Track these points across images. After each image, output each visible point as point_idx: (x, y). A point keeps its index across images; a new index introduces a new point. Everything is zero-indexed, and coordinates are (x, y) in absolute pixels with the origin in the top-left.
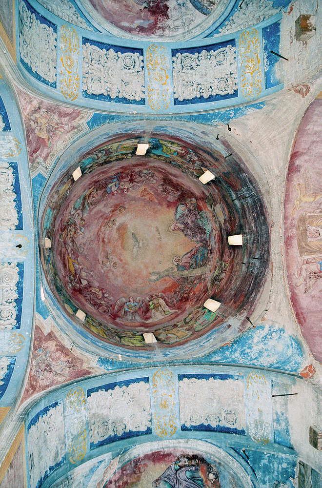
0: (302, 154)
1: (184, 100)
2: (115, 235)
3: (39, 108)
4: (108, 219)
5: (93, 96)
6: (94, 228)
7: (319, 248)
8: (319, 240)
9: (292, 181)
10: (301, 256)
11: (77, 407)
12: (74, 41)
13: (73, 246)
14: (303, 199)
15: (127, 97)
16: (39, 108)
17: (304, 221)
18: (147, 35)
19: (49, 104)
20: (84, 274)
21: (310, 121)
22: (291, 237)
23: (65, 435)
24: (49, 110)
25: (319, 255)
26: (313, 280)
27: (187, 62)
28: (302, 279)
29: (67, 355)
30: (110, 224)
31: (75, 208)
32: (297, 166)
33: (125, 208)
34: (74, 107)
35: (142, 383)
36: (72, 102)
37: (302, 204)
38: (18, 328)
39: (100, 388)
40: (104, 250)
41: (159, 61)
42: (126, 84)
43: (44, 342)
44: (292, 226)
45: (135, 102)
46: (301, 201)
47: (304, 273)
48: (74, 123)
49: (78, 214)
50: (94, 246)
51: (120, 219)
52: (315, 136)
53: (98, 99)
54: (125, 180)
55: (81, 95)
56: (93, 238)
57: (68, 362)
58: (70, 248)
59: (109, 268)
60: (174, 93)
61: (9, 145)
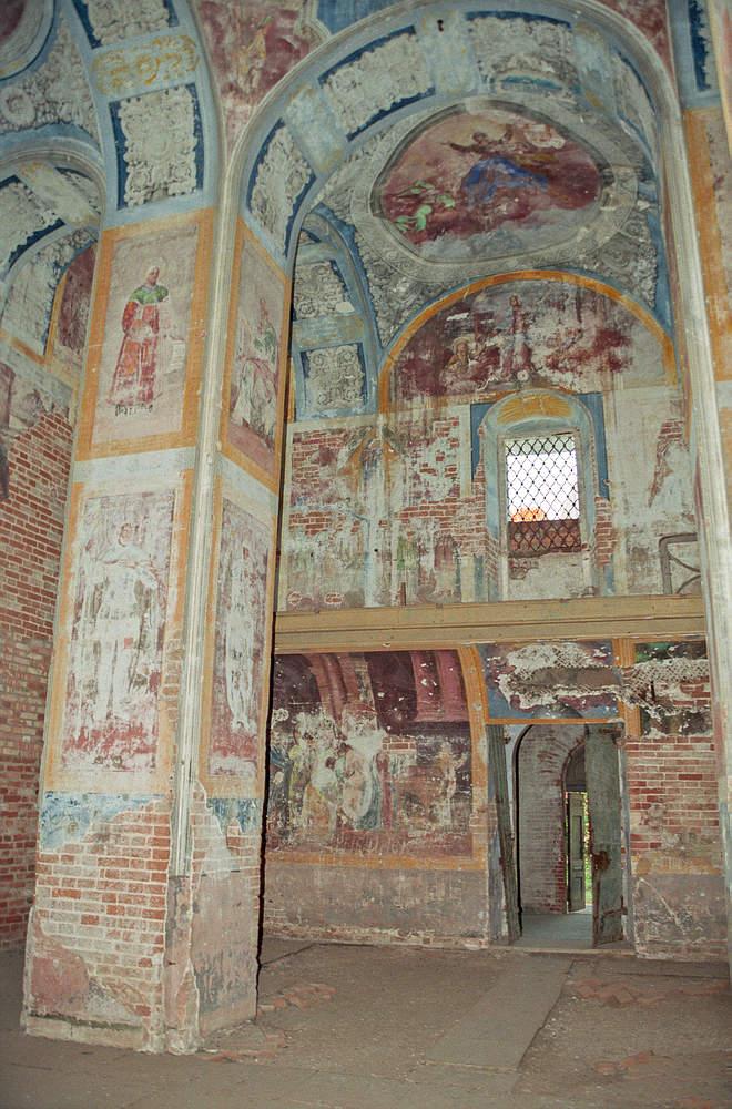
3: (231, 87)
12: (110, 64)
16: (231, 87)
34: (200, 23)
38: (568, 25)
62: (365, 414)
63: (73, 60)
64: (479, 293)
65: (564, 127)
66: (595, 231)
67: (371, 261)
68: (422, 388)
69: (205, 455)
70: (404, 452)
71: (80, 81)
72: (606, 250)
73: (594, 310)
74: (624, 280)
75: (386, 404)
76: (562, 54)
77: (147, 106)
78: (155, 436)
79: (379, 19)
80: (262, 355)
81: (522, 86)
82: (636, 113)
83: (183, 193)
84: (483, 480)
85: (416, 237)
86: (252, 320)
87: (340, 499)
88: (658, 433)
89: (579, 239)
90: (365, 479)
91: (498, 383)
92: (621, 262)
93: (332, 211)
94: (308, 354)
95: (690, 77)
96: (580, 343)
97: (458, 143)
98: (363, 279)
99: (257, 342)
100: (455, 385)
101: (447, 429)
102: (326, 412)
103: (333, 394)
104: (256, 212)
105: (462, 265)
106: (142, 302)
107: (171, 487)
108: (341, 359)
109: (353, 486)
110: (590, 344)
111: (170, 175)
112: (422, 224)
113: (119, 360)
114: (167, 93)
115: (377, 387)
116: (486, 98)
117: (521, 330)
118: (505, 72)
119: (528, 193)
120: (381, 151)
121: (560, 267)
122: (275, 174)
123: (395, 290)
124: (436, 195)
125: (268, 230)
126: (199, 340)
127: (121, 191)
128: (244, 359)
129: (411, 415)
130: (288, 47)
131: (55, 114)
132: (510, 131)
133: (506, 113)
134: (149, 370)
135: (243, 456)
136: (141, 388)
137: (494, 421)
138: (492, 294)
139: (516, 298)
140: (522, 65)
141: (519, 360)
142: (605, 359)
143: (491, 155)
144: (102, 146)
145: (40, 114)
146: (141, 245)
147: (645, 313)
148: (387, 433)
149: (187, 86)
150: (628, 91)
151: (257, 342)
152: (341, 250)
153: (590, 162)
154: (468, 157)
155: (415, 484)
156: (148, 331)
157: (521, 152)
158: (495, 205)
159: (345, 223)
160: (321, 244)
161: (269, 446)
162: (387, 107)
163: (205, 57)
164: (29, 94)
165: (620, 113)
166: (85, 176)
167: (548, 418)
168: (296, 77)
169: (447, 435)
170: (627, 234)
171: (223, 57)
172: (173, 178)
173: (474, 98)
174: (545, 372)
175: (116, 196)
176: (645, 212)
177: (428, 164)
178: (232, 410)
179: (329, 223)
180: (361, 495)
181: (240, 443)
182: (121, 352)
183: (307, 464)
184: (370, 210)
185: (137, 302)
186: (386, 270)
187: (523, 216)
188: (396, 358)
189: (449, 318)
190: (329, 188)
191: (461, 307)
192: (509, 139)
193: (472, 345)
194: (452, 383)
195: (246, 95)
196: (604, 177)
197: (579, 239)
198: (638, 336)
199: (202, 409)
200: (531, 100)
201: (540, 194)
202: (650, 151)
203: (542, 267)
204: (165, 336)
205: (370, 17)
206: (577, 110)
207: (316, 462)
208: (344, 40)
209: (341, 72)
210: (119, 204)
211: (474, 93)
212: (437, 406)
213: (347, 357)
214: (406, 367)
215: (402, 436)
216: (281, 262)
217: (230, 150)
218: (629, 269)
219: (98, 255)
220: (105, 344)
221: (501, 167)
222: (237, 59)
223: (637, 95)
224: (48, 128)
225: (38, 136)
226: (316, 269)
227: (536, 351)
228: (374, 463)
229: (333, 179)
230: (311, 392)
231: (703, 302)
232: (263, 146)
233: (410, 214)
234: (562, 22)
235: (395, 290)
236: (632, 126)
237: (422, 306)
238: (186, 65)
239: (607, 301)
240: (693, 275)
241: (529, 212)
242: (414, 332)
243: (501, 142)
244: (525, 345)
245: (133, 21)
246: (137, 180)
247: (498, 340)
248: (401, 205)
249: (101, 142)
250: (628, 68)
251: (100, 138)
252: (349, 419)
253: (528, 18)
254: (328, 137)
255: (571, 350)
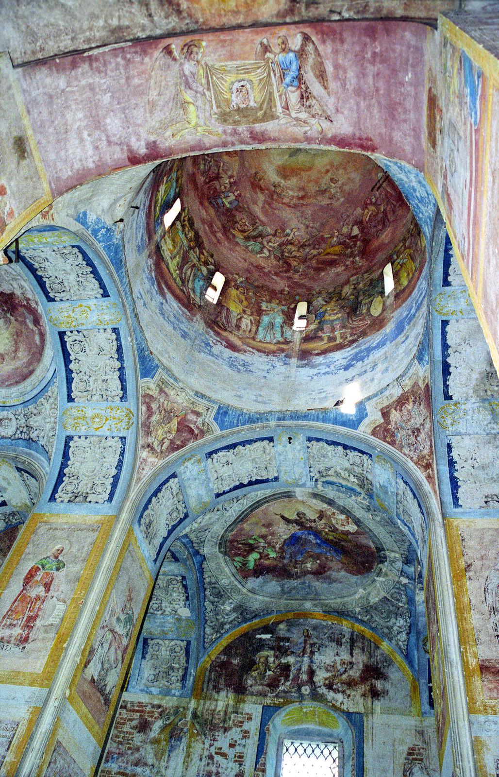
0: (130, 151)
1: (101, 288)
2: (293, 181)
3: (148, 446)
4: (273, 194)
5: (124, 388)
6: (287, 214)
7: (264, 86)
8: (252, 88)
9: (170, 148)
10: (278, 118)
11: (461, 415)
12: (75, 412)
13: (309, 245)
14: (193, 123)
15: (115, 348)
16: (148, 446)
17: (225, 114)
18: (41, 317)
19: (142, 437)
20: (345, 230)
21: (84, 169)
22: (251, 133)
23: (487, 434)
24: (148, 433)
25: (275, 87)
26: (313, 102)
27: (57, 287)
28: (313, 121)
29: (407, 399)
30: (278, 190)
31: (261, 252)
32: (147, 149)
33: (256, 174)
34: (140, 405)
35: (448, 328)
36: (135, 415)
37: (202, 123)
38: (371, 456)
39: (445, 381)
40: (315, 197)
41: (66, 314)
42: (101, 350)
43: (390, 427)
44: (235, 133)
45: (118, 339)
46: (197, 125)
47: (303, 116)
48: (154, 392)
49: (268, 243)
50: (309, 212)
51: (273, 177)
52: (100, 147)
53: (126, 382)
54: (218, 187)
55: (126, 404)
56: (298, 214)
57: (414, 402)
58: (312, 251)
59: (339, 190)
60: (96, 298)
61: (190, 466)
62: (181, 696)
63: (53, 406)
64: (282, 622)
65: (358, 519)
66: (369, 593)
67: (210, 583)
68: (228, 685)
69: (54, 697)
70: (205, 735)
71: (53, 419)
72: (375, 607)
73: (363, 649)
74: (386, 631)
75: (198, 692)
76: (365, 472)
77: (90, 443)
78: (19, 672)
79: (252, 429)
80: (120, 630)
81: (335, 487)
82: (410, 516)
83: (97, 502)
84: (264, 771)
85: (245, 573)
86: (119, 602)
87: (145, 764)
88: (405, 755)
89: (357, 596)
90: (170, 751)
91: (286, 692)
92: (385, 618)
93: (192, 542)
94: (149, 641)
95: (448, 499)
96: (351, 673)
97: (286, 515)
98: (202, 594)
99: (118, 619)
100: (253, 688)
101: (242, 722)
102: (152, 689)
103: (160, 676)
104: (143, 527)
105: (273, 600)
106: (43, 567)
107: (17, 719)
108: (172, 650)
109: (159, 756)
110: (358, 675)
111: (92, 489)
112: (251, 565)
113: (11, 607)
114: (106, 439)
115: (195, 677)
116: (311, 491)
117: (308, 654)
118: (325, 477)
119: (327, 558)
120: (234, 510)
121: (342, 613)
122: (162, 506)
123: (222, 607)
124: (264, 547)
125: (147, 542)
126: (78, 605)
127: (55, 491)
128: (106, 629)
129: (216, 706)
130: (191, 431)
131: (28, 435)
132: (322, 515)
133: (321, 503)
134: (32, 619)
135: (83, 707)
136: (21, 631)
137: (279, 723)
138: (291, 624)
139: (308, 630)
140: (337, 474)
141: (304, 677)
142: (368, 688)
143: (306, 528)
144: (52, 460)
145: (18, 432)
146: (56, 529)
147: (399, 658)
148: (195, 716)
149: (121, 438)
150: (405, 502)
151: (118, 619)
152: (191, 570)
153: (372, 546)
154: (291, 526)
155: (208, 764)
156: (40, 591)
157: (327, 530)
158: (303, 562)
159: (199, 553)
160: (179, 563)
161: (106, 704)
162: (246, 482)
163: (138, 423)
164: (17, 419)
165: (398, 515)
166: (33, 476)
167: (321, 728)
168: (192, 449)
169: (241, 726)
170: (390, 599)
171: (149, 427)
172: (93, 491)
173: (303, 489)
174: (323, 690)
175: (51, 492)
176: (405, 585)
177: (264, 525)
178: (86, 666)
179: (188, 550)
180: (163, 764)
181: (85, 697)
182: (16, 601)
183: (126, 728)
184: (217, 548)
185: (40, 567)
186: (220, 592)
187: (320, 573)
188: (213, 658)
189: (258, 636)
190: (195, 525)
191: (266, 629)
192: (321, 520)
193: (271, 659)
194: (251, 686)
195: (157, 453)
196: (380, 557)
197: (357, 596)
198: (394, 674)
199: (63, 660)
200: (339, 498)
201: (335, 562)
202: (417, 542)
203: (329, 612)
204: (53, 597)
205: (246, 427)
206: (368, 509)
207: (135, 728)
208: (227, 436)
209: (220, 454)
210: (50, 499)
211: (303, 485)
212: (238, 702)
213: (177, 649)
214: (219, 667)
215: (206, 720)
216: (150, 566)
217: (137, 483)
218: (390, 624)
219: (21, 532)
220: (6, 592)
221: (311, 538)
222: (157, 430)
223: (412, 505)
224: (20, 441)
225: (12, 445)
226: (170, 581)
227: (318, 672)
228: (180, 739)
229: (199, 520)
230: (146, 669)
231: (457, 649)
232: (159, 486)
233: (244, 556)
234: (367, 454)
235: (222, 607)
236: (406, 525)
237: (240, 624)
238: (124, 425)
239: (373, 645)
240: (451, 629)
241: (325, 572)
242: (230, 641)
243: (315, 521)
244: (310, 666)
245: (99, 392)
246: (68, 485)
247: (291, 659)
248: (239, 549)
249: (52, 458)
250: (408, 488)
251: (53, 455)
252: (168, 698)
253: (345, 447)
254: (203, 492)
255: (344, 677)
